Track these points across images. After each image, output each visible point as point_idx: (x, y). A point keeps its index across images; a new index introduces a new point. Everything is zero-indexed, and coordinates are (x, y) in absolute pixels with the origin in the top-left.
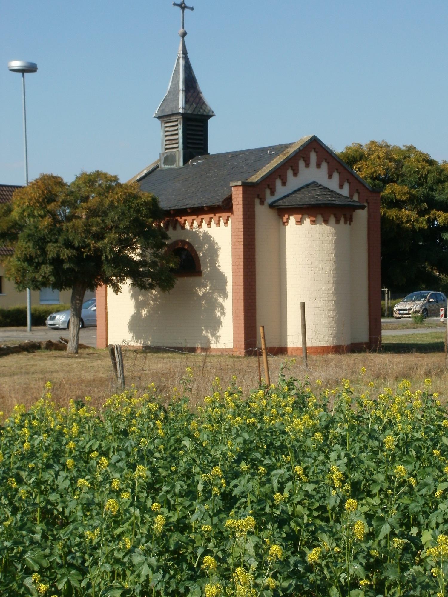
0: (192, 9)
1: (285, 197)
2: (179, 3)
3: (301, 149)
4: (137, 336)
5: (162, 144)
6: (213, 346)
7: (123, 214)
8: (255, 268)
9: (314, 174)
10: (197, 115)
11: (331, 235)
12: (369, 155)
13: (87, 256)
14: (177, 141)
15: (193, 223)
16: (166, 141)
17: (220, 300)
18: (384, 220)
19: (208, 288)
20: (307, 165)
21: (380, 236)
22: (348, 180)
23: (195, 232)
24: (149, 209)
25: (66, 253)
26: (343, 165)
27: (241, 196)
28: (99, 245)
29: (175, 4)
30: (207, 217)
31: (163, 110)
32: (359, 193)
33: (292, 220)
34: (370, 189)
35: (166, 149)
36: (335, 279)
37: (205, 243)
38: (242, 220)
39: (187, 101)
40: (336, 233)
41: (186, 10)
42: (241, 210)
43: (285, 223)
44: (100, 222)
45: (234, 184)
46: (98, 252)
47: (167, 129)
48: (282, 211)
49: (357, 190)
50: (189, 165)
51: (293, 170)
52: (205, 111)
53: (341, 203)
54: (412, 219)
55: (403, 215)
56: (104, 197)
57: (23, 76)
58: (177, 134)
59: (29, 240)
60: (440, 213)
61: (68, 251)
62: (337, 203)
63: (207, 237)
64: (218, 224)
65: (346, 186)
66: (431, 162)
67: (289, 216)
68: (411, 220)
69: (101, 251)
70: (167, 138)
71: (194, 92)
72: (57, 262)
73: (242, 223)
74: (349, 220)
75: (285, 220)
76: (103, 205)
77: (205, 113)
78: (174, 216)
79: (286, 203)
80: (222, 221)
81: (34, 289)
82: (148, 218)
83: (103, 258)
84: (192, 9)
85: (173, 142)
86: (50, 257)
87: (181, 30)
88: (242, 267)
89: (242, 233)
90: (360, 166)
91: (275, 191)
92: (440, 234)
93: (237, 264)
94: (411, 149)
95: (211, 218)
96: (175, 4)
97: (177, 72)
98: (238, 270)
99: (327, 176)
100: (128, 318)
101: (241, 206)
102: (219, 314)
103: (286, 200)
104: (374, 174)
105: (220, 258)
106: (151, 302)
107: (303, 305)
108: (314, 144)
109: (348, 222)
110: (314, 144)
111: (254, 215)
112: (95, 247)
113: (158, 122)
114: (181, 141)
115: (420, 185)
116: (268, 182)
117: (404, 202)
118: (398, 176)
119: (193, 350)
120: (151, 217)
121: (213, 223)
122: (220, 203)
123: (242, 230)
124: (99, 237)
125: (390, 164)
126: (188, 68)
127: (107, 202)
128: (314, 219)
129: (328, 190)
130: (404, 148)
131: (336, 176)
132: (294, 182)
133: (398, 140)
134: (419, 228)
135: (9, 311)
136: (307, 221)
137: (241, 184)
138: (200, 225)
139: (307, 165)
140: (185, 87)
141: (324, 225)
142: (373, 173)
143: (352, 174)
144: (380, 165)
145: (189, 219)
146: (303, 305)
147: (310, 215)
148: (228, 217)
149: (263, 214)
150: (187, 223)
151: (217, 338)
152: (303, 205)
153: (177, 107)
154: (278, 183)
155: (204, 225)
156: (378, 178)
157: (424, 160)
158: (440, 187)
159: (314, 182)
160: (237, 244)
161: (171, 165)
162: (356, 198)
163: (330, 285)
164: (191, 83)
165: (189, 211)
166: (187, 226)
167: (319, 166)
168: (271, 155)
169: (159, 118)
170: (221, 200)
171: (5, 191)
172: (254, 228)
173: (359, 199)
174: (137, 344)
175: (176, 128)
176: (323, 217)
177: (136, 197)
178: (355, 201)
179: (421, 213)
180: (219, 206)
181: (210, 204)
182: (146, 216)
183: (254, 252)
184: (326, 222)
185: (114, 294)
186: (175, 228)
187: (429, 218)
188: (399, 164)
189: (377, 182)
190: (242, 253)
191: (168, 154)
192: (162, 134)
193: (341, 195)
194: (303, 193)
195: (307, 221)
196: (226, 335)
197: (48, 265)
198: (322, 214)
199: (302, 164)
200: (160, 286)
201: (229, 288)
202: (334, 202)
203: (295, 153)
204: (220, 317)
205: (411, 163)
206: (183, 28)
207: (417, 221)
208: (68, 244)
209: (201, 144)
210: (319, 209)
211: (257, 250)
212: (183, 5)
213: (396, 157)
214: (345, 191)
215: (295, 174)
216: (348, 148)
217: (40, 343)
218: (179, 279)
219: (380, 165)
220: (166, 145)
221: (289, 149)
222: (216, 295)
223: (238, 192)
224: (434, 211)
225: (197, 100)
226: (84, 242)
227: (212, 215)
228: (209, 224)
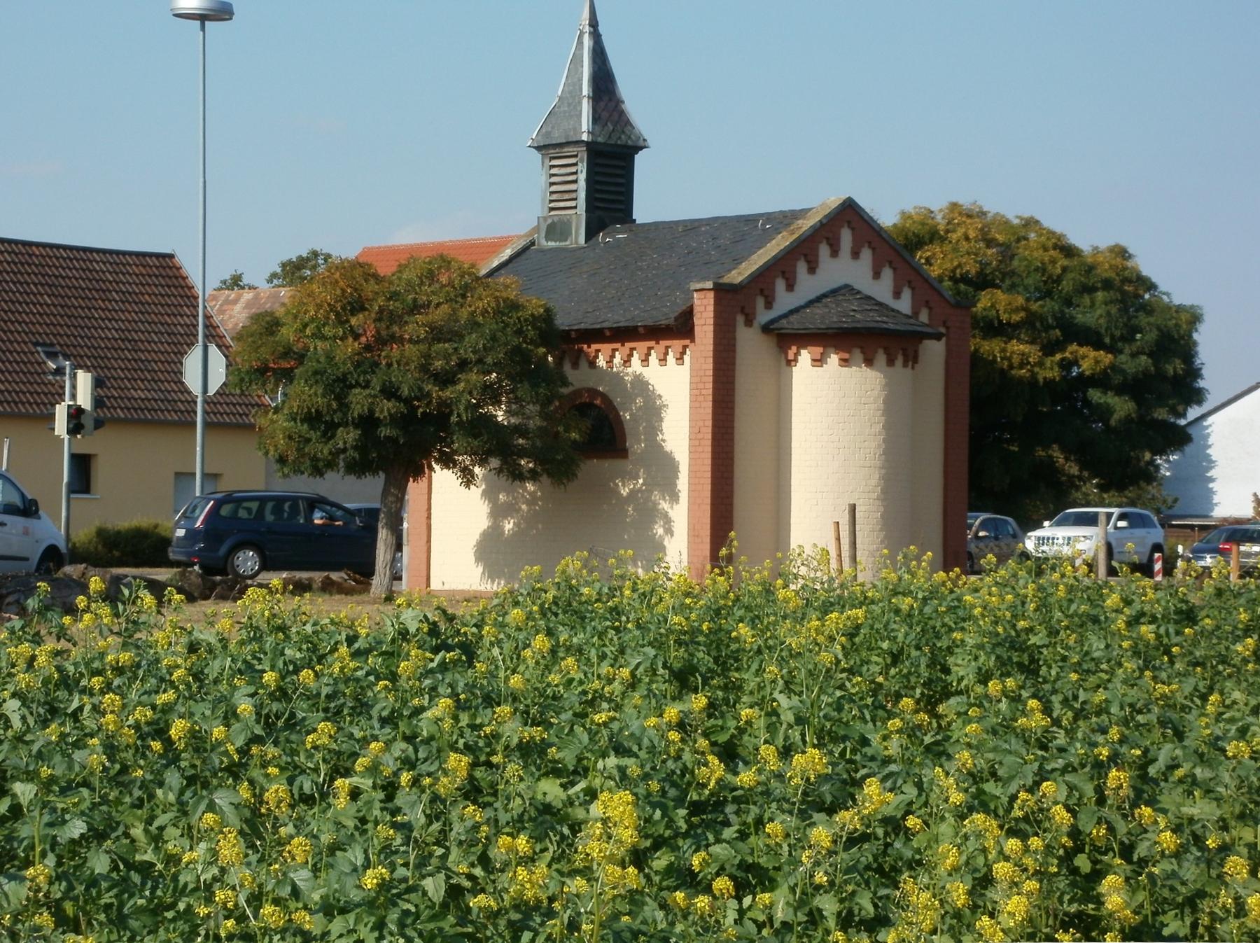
1: (792, 312)
4: (492, 572)
5: (543, 200)
7: (494, 338)
9: (846, 269)
10: (616, 145)
12: (947, 231)
13: (424, 413)
14: (573, 195)
15: (613, 356)
16: (552, 193)
17: (664, 505)
18: (976, 359)
19: (641, 481)
20: (835, 253)
22: (909, 282)
23: (618, 373)
24: (539, 329)
25: (386, 407)
26: (899, 249)
27: (711, 308)
28: (448, 393)
30: (642, 346)
31: (548, 134)
32: (930, 309)
33: (805, 356)
34: (952, 300)
36: (883, 471)
37: (637, 396)
38: (711, 354)
39: (596, 119)
40: (887, 385)
42: (711, 335)
43: (790, 363)
44: (451, 351)
45: (699, 286)
46: (445, 408)
47: (554, 171)
48: (785, 339)
49: (927, 302)
51: (808, 262)
55: (1013, 353)
56: (458, 306)
57: (203, 28)
58: (575, 182)
59: (317, 382)
60: (1083, 350)
61: (390, 405)
62: (892, 326)
63: (641, 384)
64: (663, 360)
65: (907, 294)
66: (1070, 251)
68: (1029, 363)
69: (449, 406)
70: (554, 188)
71: (610, 100)
72: (368, 423)
73: (711, 360)
74: (912, 359)
75: (791, 357)
76: (457, 321)
77: (630, 143)
78: (574, 342)
79: (795, 323)
80: (671, 354)
81: (1196, 396)
82: (537, 346)
83: (454, 419)
85: (566, 196)
86: (356, 415)
88: (709, 443)
89: (711, 379)
90: (929, 254)
91: (774, 299)
92: (1085, 393)
93: (700, 436)
94: (1030, 223)
95: (650, 349)
97: (577, 60)
98: (700, 449)
99: (871, 273)
100: (475, 536)
101: (712, 328)
102: (660, 531)
103: (793, 318)
104: (958, 271)
105: (665, 425)
106: (524, 507)
107: (853, 509)
108: (849, 213)
110: (849, 213)
112: (440, 397)
113: (537, 156)
114: (582, 195)
115: (1048, 294)
116: (762, 283)
117: (1016, 326)
118: (1004, 275)
120: (542, 345)
121: (653, 358)
122: (671, 322)
123: (711, 373)
124: (445, 379)
125: (989, 252)
126: (599, 54)
127: (464, 314)
128: (846, 356)
130: (1016, 221)
131: (887, 274)
132: (809, 285)
133: (1007, 201)
134: (1045, 378)
135: (119, 532)
136: (834, 359)
138: (627, 362)
139: (835, 253)
142: (956, 268)
143: (917, 271)
144: (968, 253)
145: (606, 348)
146: (853, 509)
147: (838, 349)
148: (685, 347)
149: (749, 341)
150: (601, 357)
153: (577, 128)
154: (780, 285)
155: (636, 360)
156: (965, 279)
157: (1055, 247)
158: (1087, 300)
159: (846, 286)
160: (701, 398)
162: (924, 317)
163: (874, 482)
164: (604, 84)
165: (608, 333)
166: (602, 362)
167: (856, 254)
168: (764, 230)
169: (539, 148)
170: (673, 316)
171: (130, 265)
172: (734, 370)
173: (930, 319)
175: (573, 169)
176: (863, 352)
177: (515, 306)
178: (924, 325)
179: (1050, 348)
180: (668, 326)
181: (650, 322)
182: (532, 342)
183: (732, 415)
184: (869, 362)
185: (463, 487)
186: (575, 365)
187: (1063, 359)
188: (1007, 252)
189: (962, 287)
190: (710, 417)
191: (556, 219)
192: (543, 179)
193: (898, 312)
194: (826, 306)
195: (834, 359)
197: (351, 428)
198: (861, 348)
199: (824, 250)
200: (550, 475)
201: (683, 483)
202: (885, 326)
205: (1031, 252)
207: (1040, 364)
208: (390, 392)
209: (620, 202)
210: (856, 338)
211: (738, 411)
213: (1000, 238)
214: (904, 305)
215: (812, 270)
216: (905, 216)
218: (589, 462)
219: (968, 253)
220: (551, 201)
221: (800, 222)
222: (656, 495)
223: (705, 302)
224: (1074, 347)
226: (421, 389)
227: (652, 343)
228: (645, 361)
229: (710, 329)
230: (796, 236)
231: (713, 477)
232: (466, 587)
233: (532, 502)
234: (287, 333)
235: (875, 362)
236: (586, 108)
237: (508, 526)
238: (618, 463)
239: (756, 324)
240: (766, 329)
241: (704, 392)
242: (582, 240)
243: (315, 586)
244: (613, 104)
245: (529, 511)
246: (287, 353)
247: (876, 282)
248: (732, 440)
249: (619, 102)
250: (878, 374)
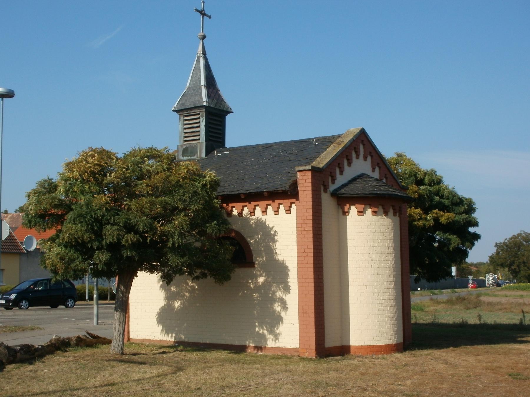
2: (200, 10)
4: (167, 330)
5: (180, 137)
6: (271, 343)
11: (391, 227)
13: (151, 240)
14: (198, 134)
17: (279, 294)
20: (358, 157)
29: (197, 10)
30: (263, 203)
31: (183, 104)
33: (353, 210)
35: (185, 141)
36: (395, 273)
39: (209, 96)
43: (345, 213)
45: (301, 168)
48: (343, 200)
50: (214, 156)
63: (262, 225)
64: (277, 212)
67: (350, 205)
69: (167, 236)
70: (186, 131)
72: (115, 248)
75: (346, 210)
77: (225, 109)
84: (210, 17)
85: (194, 134)
87: (201, 34)
88: (312, 258)
96: (197, 10)
101: (311, 192)
106: (187, 294)
109: (398, 214)
111: (321, 202)
119: (241, 349)
128: (376, 210)
131: (377, 169)
132: (349, 173)
136: (369, 211)
137: (310, 168)
138: (252, 213)
139: (358, 157)
145: (239, 205)
151: (276, 337)
152: (370, 194)
155: (258, 212)
161: (191, 156)
165: (243, 197)
166: (235, 212)
169: (178, 111)
174: (170, 339)
184: (386, 213)
191: (188, 146)
192: (180, 127)
195: (369, 211)
196: (290, 333)
199: (354, 155)
201: (293, 279)
204: (280, 313)
208: (129, 228)
217: (69, 339)
220: (185, 137)
223: (305, 177)
228: (264, 212)
229: (309, 194)
230: (342, 146)
231: (315, 279)
232: (151, 338)
233: (192, 291)
234: (60, 193)
236: (204, 91)
237: (177, 304)
238: (247, 270)
239: (328, 192)
241: (306, 229)
242: (204, 155)
243: (72, 343)
245: (190, 296)
246: (61, 204)
248: (322, 256)
249: (218, 91)
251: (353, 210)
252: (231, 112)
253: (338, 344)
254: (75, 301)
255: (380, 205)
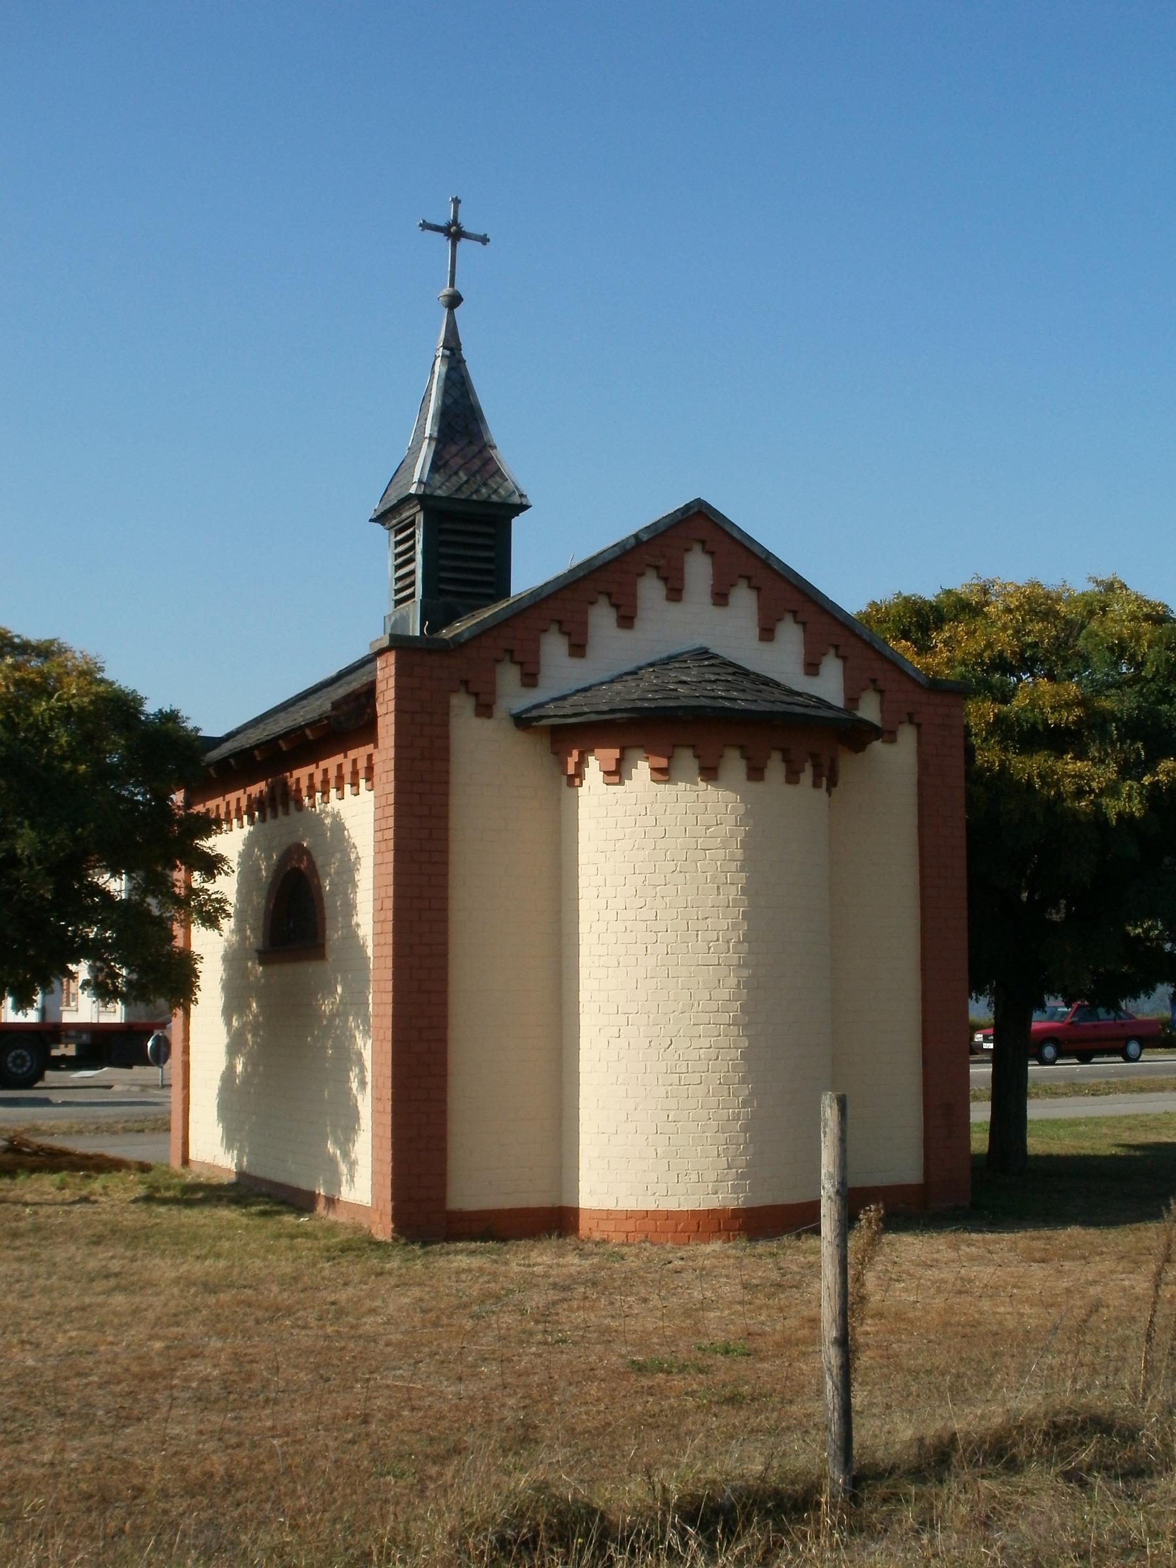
0: (484, 240)
2: (442, 223)
3: (645, 537)
8: (445, 933)
10: (468, 501)
20: (675, 593)
21: (963, 833)
29: (426, 226)
40: (747, 814)
41: (463, 243)
48: (568, 736)
52: (496, 491)
53: (753, 707)
54: (1094, 784)
75: (571, 770)
77: (494, 498)
84: (484, 240)
87: (447, 290)
96: (426, 226)
126: (457, 384)
128: (662, 762)
129: (731, 670)
136: (642, 770)
139: (675, 593)
140: (440, 431)
141: (702, 785)
147: (650, 750)
149: (483, 748)
152: (612, 711)
167: (720, 598)
176: (747, 757)
184: (710, 773)
188: (1073, 628)
195: (642, 770)
202: (727, 704)
203: (618, 552)
206: (452, 285)
210: (680, 728)
212: (453, 229)
215: (626, 620)
225: (477, 463)
235: (767, 773)
240: (522, 722)
244: (475, 449)
247: (766, 646)
250: (730, 796)
251: (594, 769)
252: (525, 507)
253: (536, 1198)
254: (1142, 1048)
255: (774, 748)
